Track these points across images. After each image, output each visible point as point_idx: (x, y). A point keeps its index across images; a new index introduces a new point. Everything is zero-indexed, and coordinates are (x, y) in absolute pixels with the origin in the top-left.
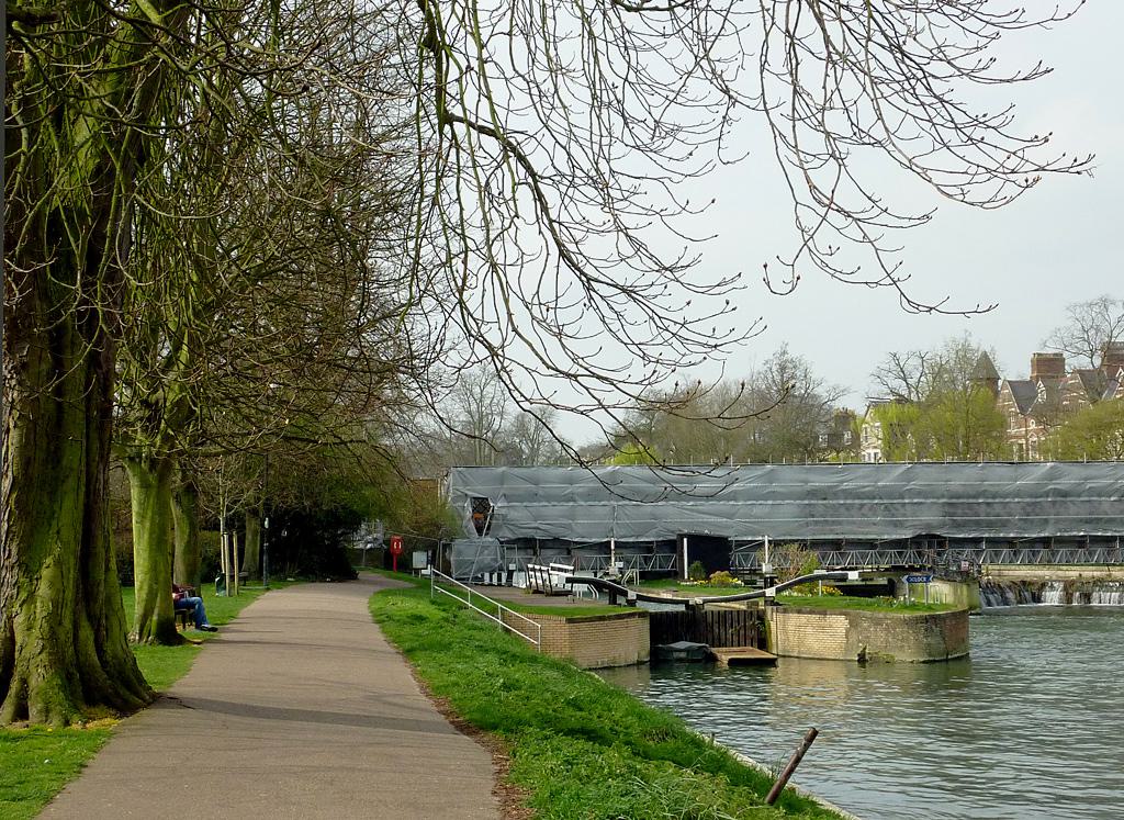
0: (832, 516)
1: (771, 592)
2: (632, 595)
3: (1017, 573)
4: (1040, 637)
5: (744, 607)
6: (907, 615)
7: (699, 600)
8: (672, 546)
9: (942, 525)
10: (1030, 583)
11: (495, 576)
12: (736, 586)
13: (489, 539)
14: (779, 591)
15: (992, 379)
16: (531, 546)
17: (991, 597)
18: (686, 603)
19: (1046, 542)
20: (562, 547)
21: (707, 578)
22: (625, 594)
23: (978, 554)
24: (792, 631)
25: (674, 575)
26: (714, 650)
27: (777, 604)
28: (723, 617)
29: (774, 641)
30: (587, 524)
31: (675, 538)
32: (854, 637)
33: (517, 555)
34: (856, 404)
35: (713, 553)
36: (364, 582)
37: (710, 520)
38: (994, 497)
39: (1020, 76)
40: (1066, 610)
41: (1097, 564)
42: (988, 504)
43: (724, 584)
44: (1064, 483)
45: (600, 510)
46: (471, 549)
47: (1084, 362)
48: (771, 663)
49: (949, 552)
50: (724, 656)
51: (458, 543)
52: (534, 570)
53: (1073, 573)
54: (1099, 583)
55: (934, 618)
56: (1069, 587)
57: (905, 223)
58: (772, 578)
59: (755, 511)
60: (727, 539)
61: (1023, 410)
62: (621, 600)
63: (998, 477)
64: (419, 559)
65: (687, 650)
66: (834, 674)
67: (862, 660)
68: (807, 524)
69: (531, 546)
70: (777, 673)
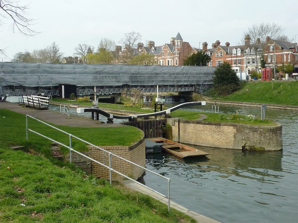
7: (135, 116)
9: (129, 82)
33: (9, 91)
37: (69, 80)
38: (142, 75)
68: (95, 82)
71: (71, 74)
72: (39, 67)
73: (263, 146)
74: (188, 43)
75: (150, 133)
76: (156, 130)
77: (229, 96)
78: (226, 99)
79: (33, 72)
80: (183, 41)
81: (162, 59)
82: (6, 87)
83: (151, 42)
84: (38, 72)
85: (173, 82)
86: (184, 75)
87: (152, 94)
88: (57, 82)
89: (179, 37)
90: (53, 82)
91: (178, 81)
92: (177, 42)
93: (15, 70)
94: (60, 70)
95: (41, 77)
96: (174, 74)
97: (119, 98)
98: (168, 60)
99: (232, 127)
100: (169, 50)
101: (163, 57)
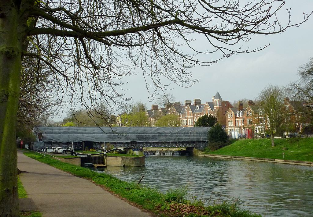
0: (114, 137)
1: (105, 153)
2: (77, 153)
3: (150, 149)
4: (175, 164)
5: (99, 156)
6: (133, 157)
7: (90, 154)
8: (81, 143)
9: (136, 139)
10: (153, 151)
11: (43, 150)
12: (95, 152)
13: (42, 142)
14: (107, 152)
15: (144, 110)
16: (51, 144)
17: (145, 154)
18: (88, 155)
19: (156, 143)
20: (58, 144)
21: (89, 150)
22: (75, 153)
23: (143, 145)
24: (109, 161)
25: (81, 150)
26: (93, 165)
27: (106, 155)
28: (95, 158)
29: (106, 162)
30: (63, 139)
31: (81, 142)
32: (122, 162)
33: (48, 145)
34: (116, 114)
35: (90, 145)
36: (198, 159)
37: (89, 138)
38: (147, 134)
39: (185, 38)
40: (160, 156)
41: (167, 147)
42: (145, 135)
43: (92, 151)
44: (160, 131)
45: (66, 136)
46: (38, 143)
47: (163, 107)
48: (105, 167)
49: (138, 145)
50: (96, 166)
51: (35, 143)
52: (53, 148)
53: (161, 149)
54: (167, 151)
55: (139, 158)
56: (160, 152)
57: (208, 64)
58: (105, 150)
59: (99, 136)
60: (93, 142)
61: (150, 116)
62: (74, 155)
63: (148, 130)
64: (27, 146)
65: (88, 165)
66: (119, 169)
67: (124, 166)
68: (109, 139)
69: (51, 144)
70: (106, 170)
71: (91, 134)
72: (69, 129)
73: (130, 165)
74: (227, 102)
75: (96, 162)
76: (99, 161)
77: (216, 151)
78: (218, 153)
79: (64, 133)
80: (222, 100)
81: (185, 118)
82: (46, 142)
83: (196, 100)
84: (68, 133)
85: (175, 139)
86: (185, 134)
87: (163, 149)
88: (81, 139)
89: (218, 96)
90: (79, 139)
91: (179, 139)
92: (216, 101)
93: (53, 132)
94: (84, 132)
95: (70, 136)
96: (175, 133)
97: (129, 152)
98: (189, 119)
99: (120, 158)
100: (209, 108)
101: (186, 117)
